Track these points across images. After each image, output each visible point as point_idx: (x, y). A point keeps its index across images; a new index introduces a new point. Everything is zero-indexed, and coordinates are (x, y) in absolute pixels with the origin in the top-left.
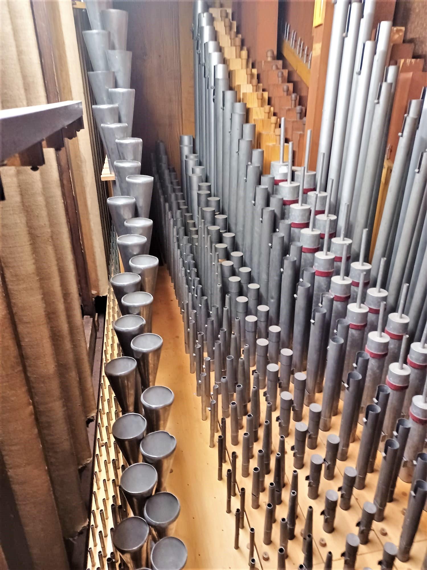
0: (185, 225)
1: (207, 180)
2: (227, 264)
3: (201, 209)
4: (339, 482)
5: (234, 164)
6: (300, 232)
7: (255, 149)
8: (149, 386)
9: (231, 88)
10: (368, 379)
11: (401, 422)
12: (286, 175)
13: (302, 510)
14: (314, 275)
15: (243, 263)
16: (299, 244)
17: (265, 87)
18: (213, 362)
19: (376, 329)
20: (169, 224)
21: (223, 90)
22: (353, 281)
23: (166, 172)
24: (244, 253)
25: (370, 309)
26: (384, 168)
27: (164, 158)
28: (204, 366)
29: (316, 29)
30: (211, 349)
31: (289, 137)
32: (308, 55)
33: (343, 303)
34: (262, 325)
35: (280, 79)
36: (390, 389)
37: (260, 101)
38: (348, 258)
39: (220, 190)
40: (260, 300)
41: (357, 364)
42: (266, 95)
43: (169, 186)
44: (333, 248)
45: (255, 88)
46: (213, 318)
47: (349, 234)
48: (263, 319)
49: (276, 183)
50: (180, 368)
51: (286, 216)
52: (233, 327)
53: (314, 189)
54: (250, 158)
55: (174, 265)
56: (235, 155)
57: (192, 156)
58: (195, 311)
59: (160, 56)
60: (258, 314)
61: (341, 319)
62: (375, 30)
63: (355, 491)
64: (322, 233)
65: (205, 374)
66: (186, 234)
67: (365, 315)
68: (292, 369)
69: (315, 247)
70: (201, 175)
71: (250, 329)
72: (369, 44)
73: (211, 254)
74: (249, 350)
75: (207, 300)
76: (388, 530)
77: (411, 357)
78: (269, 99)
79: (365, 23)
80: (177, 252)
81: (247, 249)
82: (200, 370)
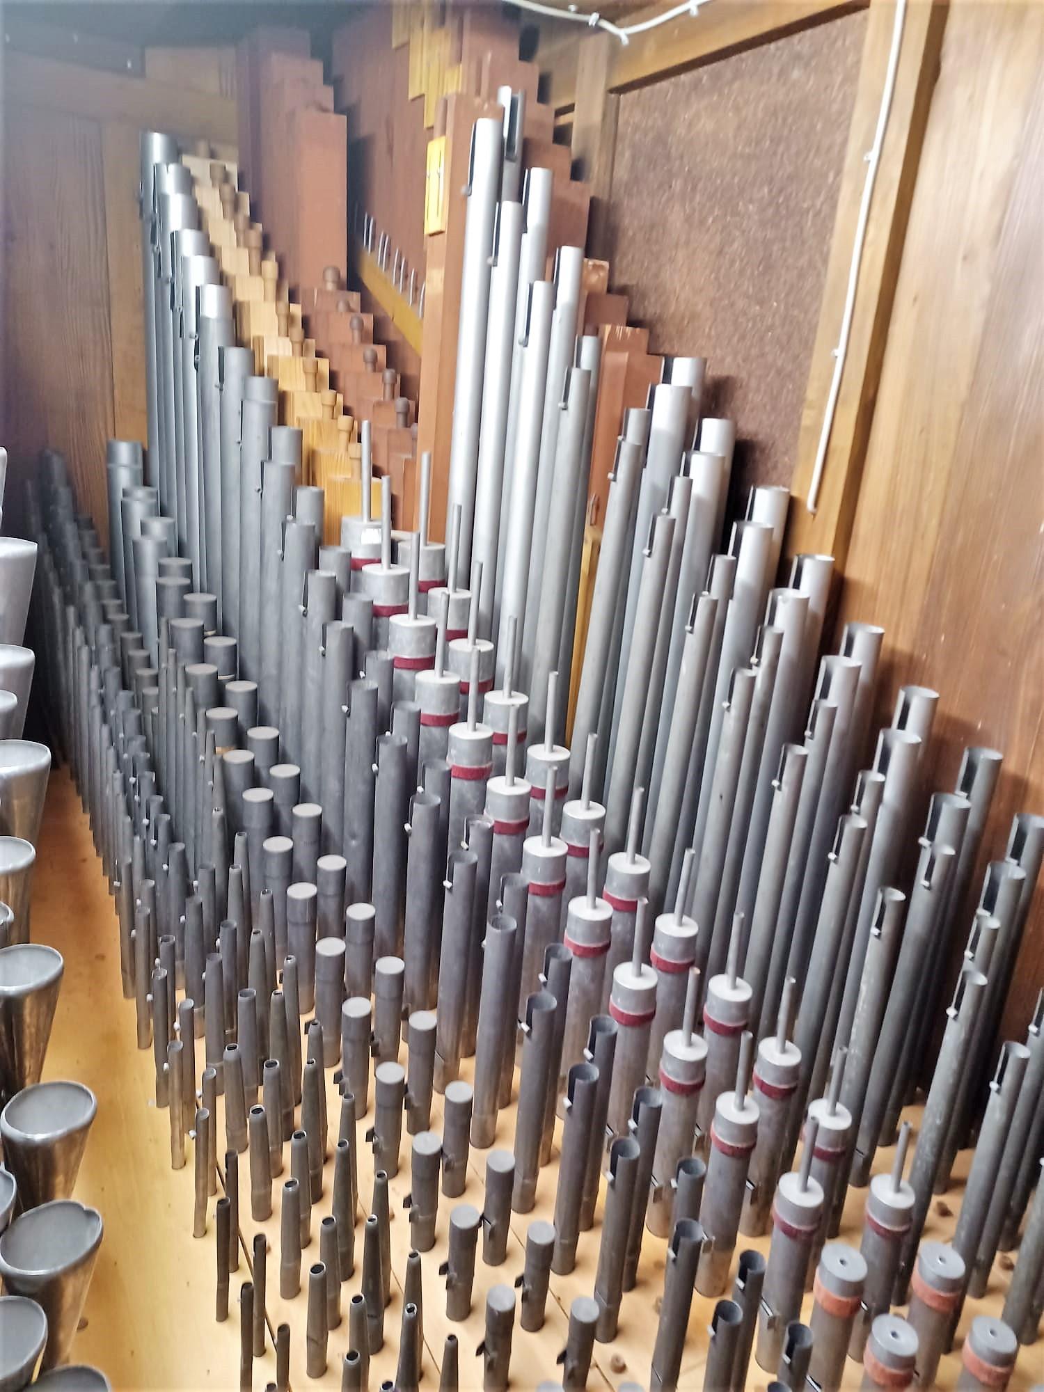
0: (123, 663)
1: (181, 551)
2: (238, 757)
3: (167, 622)
4: (518, 1265)
5: (252, 517)
6: (414, 678)
7: (304, 486)
8: (22, 1086)
9: (239, 342)
10: (572, 1008)
11: (643, 1096)
12: (378, 548)
13: (433, 1354)
14: (448, 776)
15: (278, 754)
16: (413, 707)
17: (323, 348)
18: (203, 1015)
19: (583, 892)
20: (77, 660)
21: (221, 345)
22: (533, 788)
23: (69, 529)
24: (283, 731)
25: (571, 848)
26: (587, 542)
27: (63, 493)
28: (177, 1025)
29: (432, 238)
30: (195, 979)
31: (382, 463)
32: (416, 289)
33: (514, 837)
34: (329, 907)
35: (356, 334)
36: (616, 1022)
37: (311, 378)
38: (521, 738)
39: (217, 578)
40: (323, 842)
41: (546, 975)
42: (324, 365)
43: (78, 564)
44: (488, 715)
45: (298, 347)
46: (202, 897)
47: (521, 683)
48: (331, 889)
49: (354, 566)
50: (111, 1039)
51: (382, 641)
52: (254, 918)
53: (444, 584)
54: (291, 506)
55: (91, 767)
56: (253, 497)
57: (141, 493)
58: (152, 883)
59: (52, 247)
60: (320, 879)
61: (510, 874)
62: (553, 259)
63: (555, 1280)
64: (462, 681)
65: (179, 1044)
66: (125, 685)
67: (562, 860)
68: (403, 1008)
69: (448, 714)
70: (164, 539)
71: (299, 918)
72: (541, 288)
73: (195, 733)
74: (296, 968)
75: (184, 852)
76: (627, 1358)
77: (657, 949)
78: (333, 377)
79: (530, 242)
80: (100, 734)
81: (289, 721)
82: (166, 1035)
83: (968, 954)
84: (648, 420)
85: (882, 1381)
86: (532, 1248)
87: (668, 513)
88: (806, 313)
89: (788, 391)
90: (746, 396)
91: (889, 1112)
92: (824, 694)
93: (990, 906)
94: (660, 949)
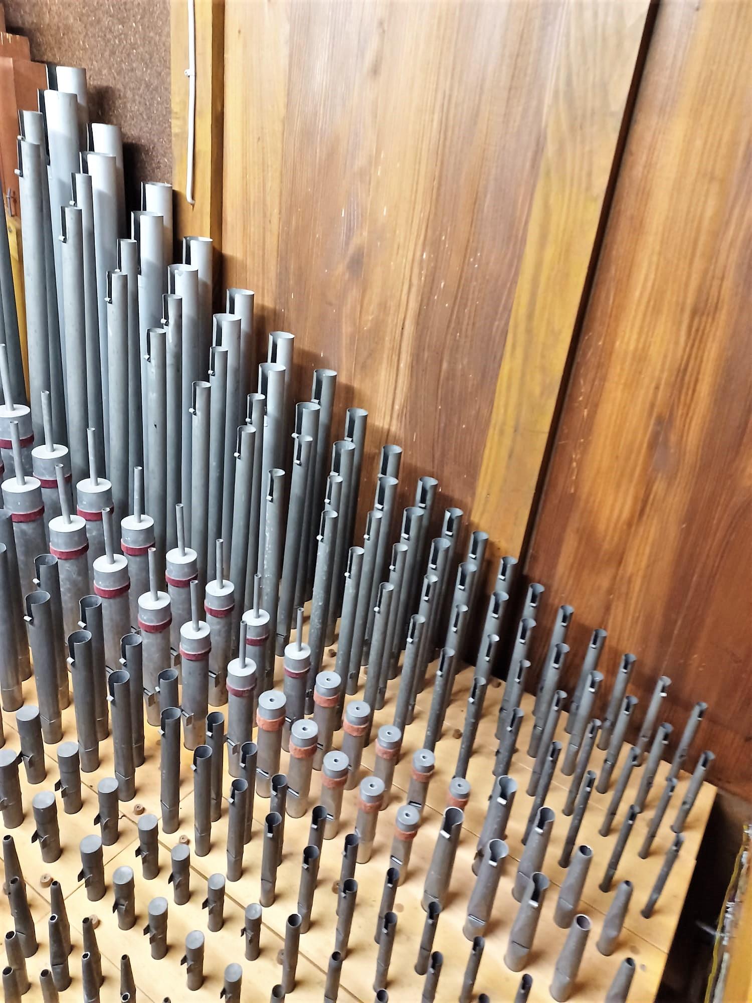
4: (92, 810)
11: (126, 641)
19: (103, 553)
77: (125, 541)
83: (327, 501)
84: (42, 122)
85: (300, 756)
86: (63, 761)
87: (75, 205)
88: (160, 35)
89: (158, 103)
90: (125, 107)
91: (330, 622)
92: (219, 343)
93: (337, 470)
94: (127, 541)
